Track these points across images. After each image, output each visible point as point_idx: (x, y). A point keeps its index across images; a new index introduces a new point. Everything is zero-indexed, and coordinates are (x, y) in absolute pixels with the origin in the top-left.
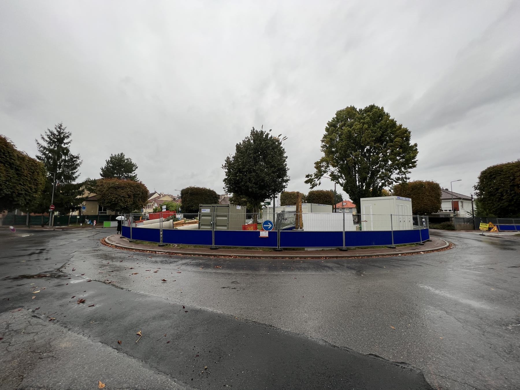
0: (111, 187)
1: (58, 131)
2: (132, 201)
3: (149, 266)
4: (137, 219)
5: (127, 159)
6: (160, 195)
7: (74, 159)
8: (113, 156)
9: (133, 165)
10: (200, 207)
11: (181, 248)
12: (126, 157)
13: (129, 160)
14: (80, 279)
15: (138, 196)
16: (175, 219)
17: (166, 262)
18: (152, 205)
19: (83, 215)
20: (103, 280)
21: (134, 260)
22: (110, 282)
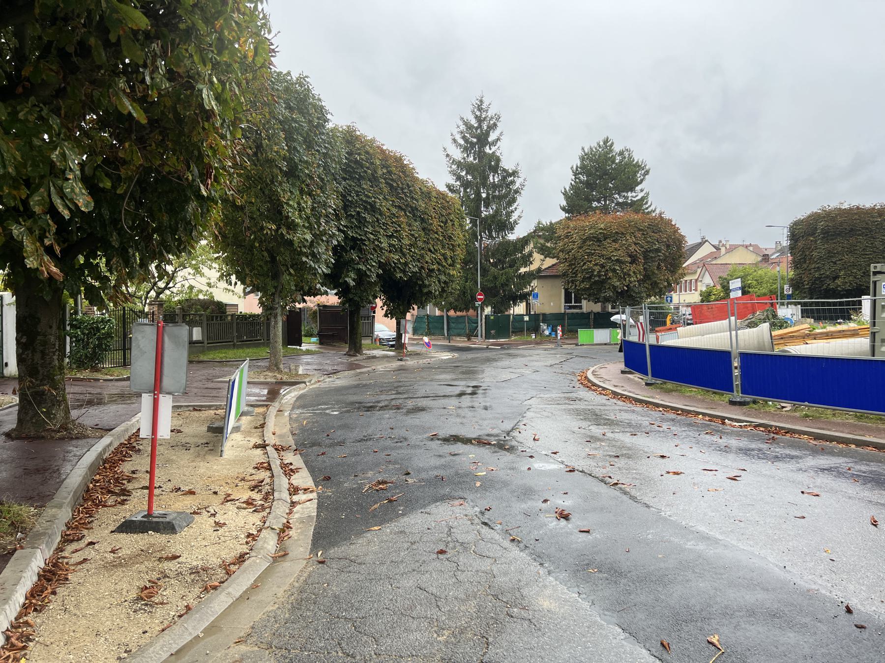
0: (589, 238)
1: (476, 117)
2: (640, 272)
3: (713, 459)
4: (658, 321)
5: (621, 153)
6: (718, 249)
7: (510, 179)
8: (586, 151)
9: (638, 166)
10: (875, 273)
11: (807, 416)
12: (617, 148)
13: (626, 154)
14: (551, 462)
15: (655, 257)
16: (778, 323)
17: (762, 455)
18: (696, 280)
19: (535, 314)
20: (600, 475)
21: (665, 435)
22: (617, 484)
